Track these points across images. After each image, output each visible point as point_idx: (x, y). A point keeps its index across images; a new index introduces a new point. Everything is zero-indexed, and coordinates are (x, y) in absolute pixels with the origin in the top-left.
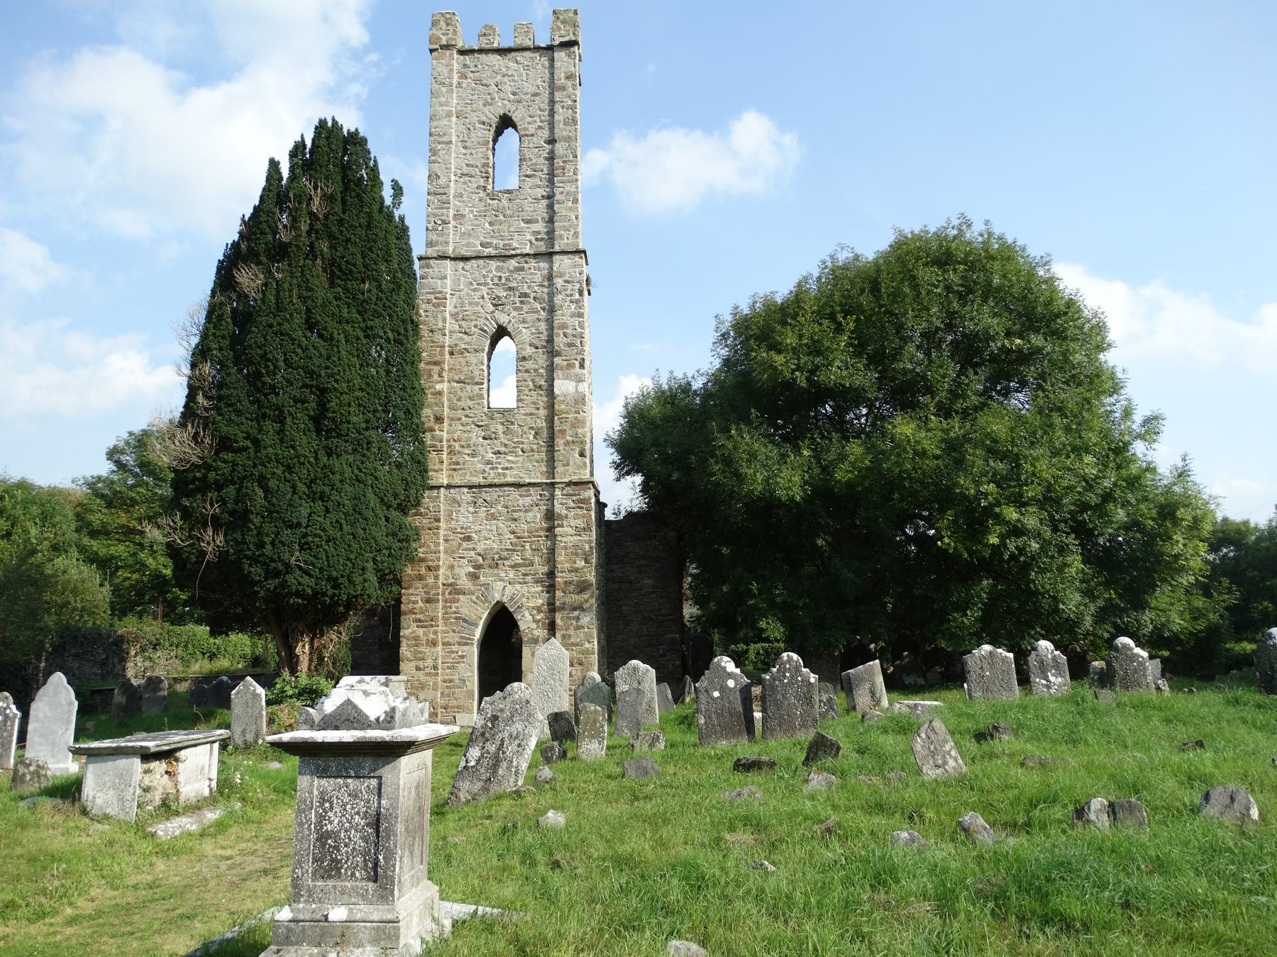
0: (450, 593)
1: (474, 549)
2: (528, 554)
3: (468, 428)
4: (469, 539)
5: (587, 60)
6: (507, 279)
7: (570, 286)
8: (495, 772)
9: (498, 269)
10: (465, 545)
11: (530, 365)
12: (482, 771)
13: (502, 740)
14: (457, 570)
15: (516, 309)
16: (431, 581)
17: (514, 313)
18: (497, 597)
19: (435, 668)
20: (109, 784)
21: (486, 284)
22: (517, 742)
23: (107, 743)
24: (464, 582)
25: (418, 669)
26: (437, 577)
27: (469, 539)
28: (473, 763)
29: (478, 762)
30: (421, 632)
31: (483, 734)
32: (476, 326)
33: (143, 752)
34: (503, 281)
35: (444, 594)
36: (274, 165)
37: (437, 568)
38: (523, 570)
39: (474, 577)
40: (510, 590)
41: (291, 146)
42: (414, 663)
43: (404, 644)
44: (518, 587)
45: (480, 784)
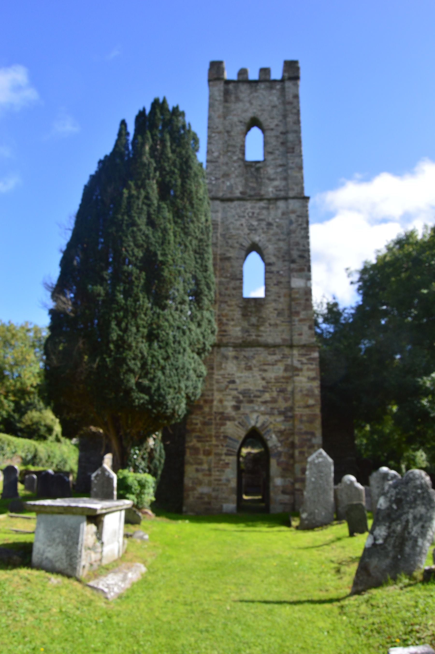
0: (220, 419)
1: (236, 389)
2: (275, 394)
3: (232, 308)
4: (233, 382)
5: (305, 88)
6: (258, 214)
7: (300, 219)
8: (401, 551)
9: (252, 208)
10: (231, 386)
11: (274, 269)
12: (390, 548)
13: (407, 521)
14: (226, 403)
15: (264, 233)
16: (206, 409)
17: (263, 235)
18: (253, 423)
19: (210, 470)
20: (58, 540)
21: (244, 217)
22: (420, 524)
23: (59, 502)
24: (230, 411)
25: (197, 470)
26: (211, 408)
27: (233, 382)
28: (380, 541)
29: (386, 539)
30: (199, 445)
31: (389, 515)
32: (237, 243)
33: (90, 513)
34: (255, 215)
35: (215, 419)
36: (123, 123)
37: (212, 401)
38: (270, 405)
39: (237, 408)
40: (262, 419)
41: (136, 113)
42: (195, 466)
43: (188, 452)
44: (267, 417)
45: (388, 561)
